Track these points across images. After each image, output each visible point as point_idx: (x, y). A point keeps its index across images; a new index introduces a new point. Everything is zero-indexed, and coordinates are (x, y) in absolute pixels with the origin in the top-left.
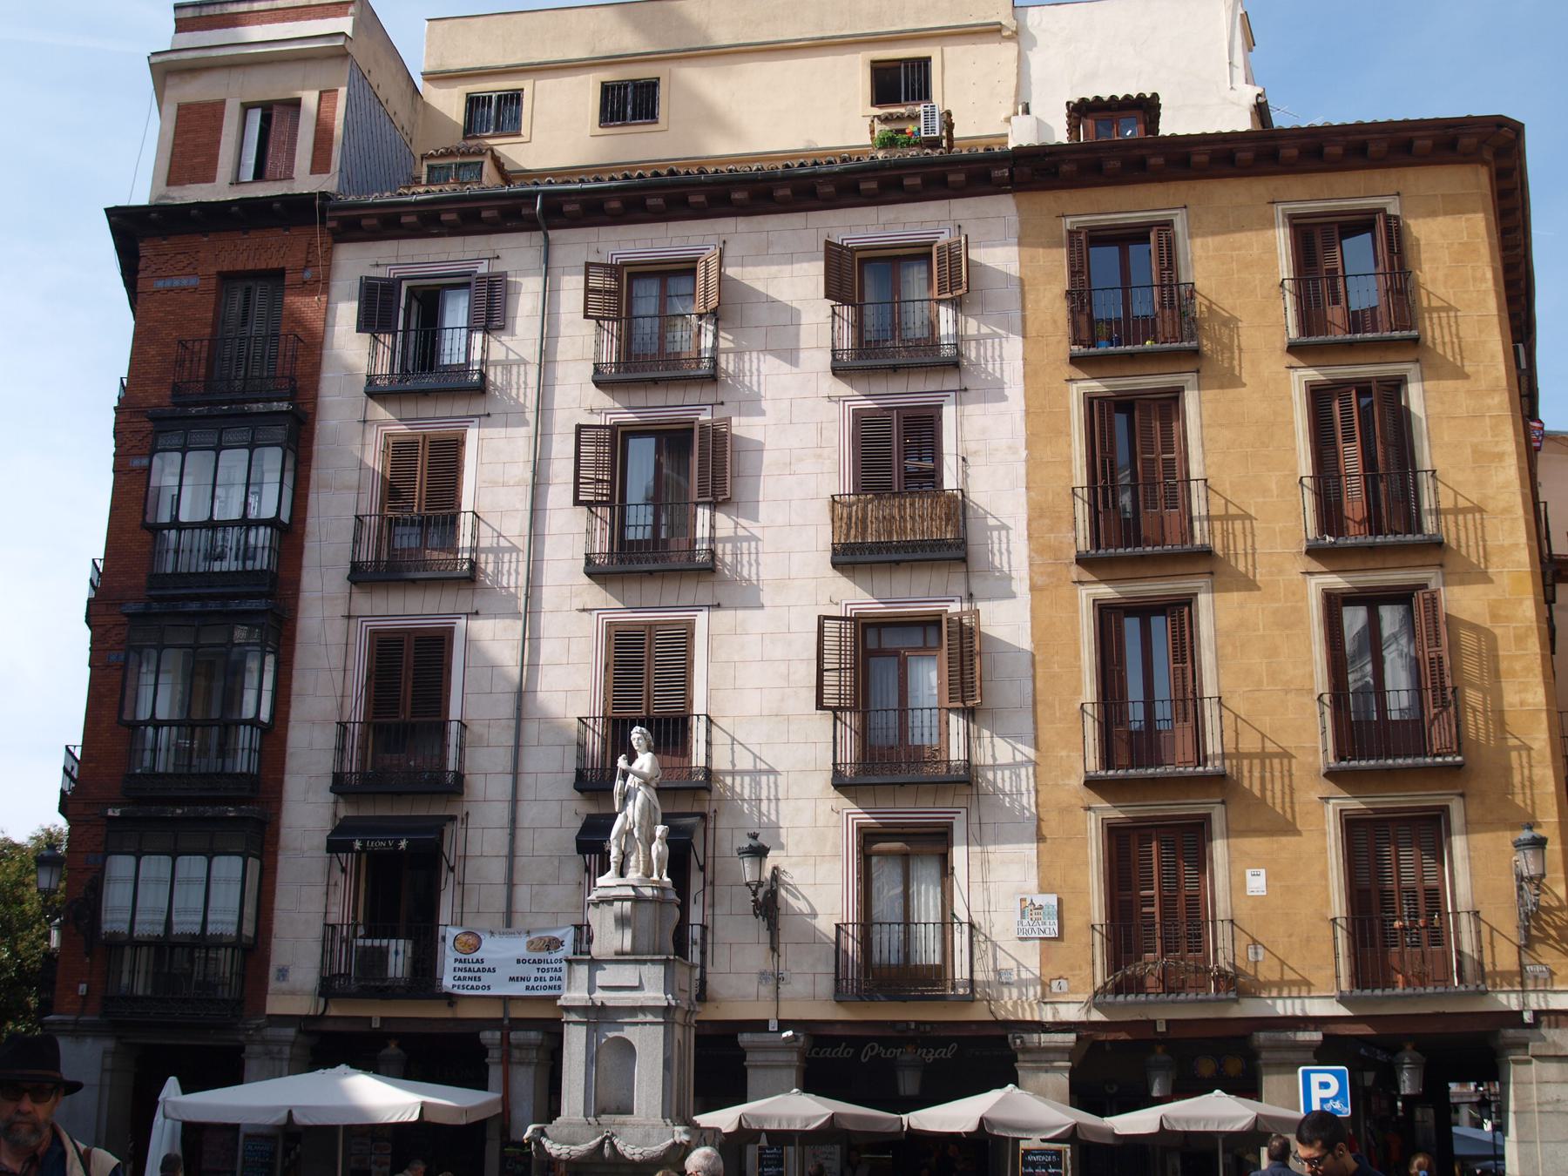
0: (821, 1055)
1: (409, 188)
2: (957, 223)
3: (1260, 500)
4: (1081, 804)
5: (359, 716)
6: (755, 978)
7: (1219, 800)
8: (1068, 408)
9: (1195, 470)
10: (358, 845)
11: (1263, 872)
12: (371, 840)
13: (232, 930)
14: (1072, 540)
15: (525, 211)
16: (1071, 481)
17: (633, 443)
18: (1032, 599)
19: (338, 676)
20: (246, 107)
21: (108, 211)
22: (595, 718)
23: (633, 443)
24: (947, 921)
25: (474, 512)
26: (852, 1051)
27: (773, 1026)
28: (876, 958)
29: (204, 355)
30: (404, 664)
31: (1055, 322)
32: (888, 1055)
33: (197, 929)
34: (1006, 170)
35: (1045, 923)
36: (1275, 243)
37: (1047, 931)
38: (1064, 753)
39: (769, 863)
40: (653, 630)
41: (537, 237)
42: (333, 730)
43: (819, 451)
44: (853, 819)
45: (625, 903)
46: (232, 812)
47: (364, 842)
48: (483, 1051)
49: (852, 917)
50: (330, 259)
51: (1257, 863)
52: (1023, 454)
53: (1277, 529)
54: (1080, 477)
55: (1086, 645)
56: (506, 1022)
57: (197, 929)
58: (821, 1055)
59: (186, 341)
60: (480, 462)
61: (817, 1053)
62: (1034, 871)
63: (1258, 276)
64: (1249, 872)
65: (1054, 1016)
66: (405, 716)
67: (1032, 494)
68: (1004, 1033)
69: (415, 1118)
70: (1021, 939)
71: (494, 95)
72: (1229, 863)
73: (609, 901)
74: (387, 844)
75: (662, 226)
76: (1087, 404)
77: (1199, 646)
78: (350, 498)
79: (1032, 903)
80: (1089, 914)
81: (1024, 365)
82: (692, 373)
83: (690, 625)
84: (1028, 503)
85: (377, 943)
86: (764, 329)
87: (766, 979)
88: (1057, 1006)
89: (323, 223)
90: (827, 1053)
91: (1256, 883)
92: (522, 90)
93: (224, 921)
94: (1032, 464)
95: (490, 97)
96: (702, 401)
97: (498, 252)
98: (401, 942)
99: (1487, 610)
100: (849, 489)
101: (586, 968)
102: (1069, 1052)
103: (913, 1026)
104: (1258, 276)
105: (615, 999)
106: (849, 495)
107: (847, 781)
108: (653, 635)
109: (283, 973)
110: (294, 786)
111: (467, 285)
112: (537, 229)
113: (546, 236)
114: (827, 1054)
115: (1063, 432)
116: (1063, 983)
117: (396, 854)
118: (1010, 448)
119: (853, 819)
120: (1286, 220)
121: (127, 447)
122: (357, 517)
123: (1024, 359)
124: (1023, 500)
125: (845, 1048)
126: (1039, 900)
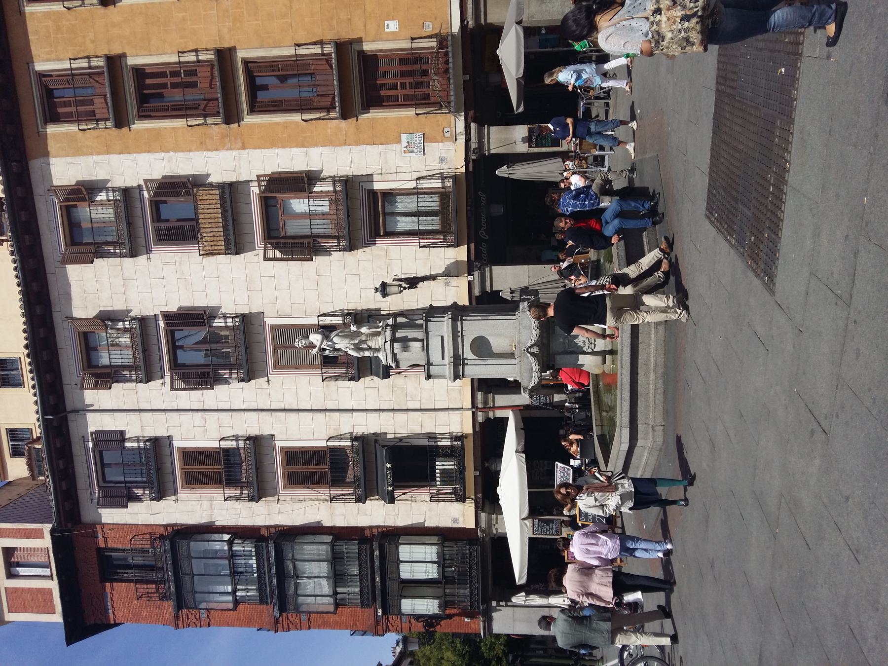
0: (486, 258)
1: (47, 487)
2: (46, 191)
3: (189, 23)
5: (327, 491)
7: (350, 46)
8: (145, 129)
9: (174, 59)
10: (390, 488)
11: (386, 22)
12: (388, 482)
13: (435, 549)
14: (217, 126)
15: (55, 424)
16: (184, 127)
17: (180, 361)
18: (250, 148)
19: (308, 503)
20: (10, 575)
21: (68, 645)
22: (322, 373)
23: (180, 361)
24: (416, 192)
25: (219, 441)
26: (483, 244)
28: (438, 227)
29: (145, 586)
30: (300, 471)
31: (98, 137)
32: (485, 226)
33: (435, 566)
34: (13, 164)
36: (44, 12)
37: (420, 139)
38: (329, 131)
39: (390, 282)
40: (277, 346)
41: (71, 417)
42: (334, 504)
43: (177, 264)
44: (368, 241)
45: (395, 346)
46: (377, 553)
47: (388, 485)
48: (488, 420)
49: (415, 240)
50: (91, 524)
51: (382, 27)
52: (172, 153)
53: (205, 13)
54: (181, 123)
55: (272, 119)
56: (474, 410)
57: (435, 566)
58: (486, 258)
59: (137, 596)
60: (194, 439)
61: (485, 260)
62: (389, 146)
63: (64, 22)
64: (387, 30)
65: (462, 135)
66: (326, 468)
67: (193, 149)
68: (471, 161)
69: (524, 455)
70: (424, 154)
71: (11, 443)
72: (382, 41)
73: (394, 356)
74: (389, 473)
75: (60, 351)
76: (141, 119)
77: (269, 57)
78: (216, 504)
79: (406, 147)
80: (411, 117)
81: (123, 154)
82: (139, 331)
83: (273, 327)
84: (198, 151)
85: (438, 475)
86: (113, 295)
87: (448, 283)
88: (457, 133)
89: (70, 531)
90: (484, 256)
91: (392, 26)
92: (6, 429)
93: (429, 552)
94: (177, 149)
95: (12, 445)
96: (155, 325)
97: (80, 438)
98: (437, 463)
100: (196, 247)
101: (431, 367)
102: (481, 125)
103: (469, 208)
104: (64, 22)
105: (449, 350)
106: (199, 247)
107: (348, 244)
108: (280, 346)
109: (455, 520)
110: (363, 520)
111: (101, 453)
112: (66, 416)
113: (70, 412)
114: (485, 255)
115: (158, 132)
116: (445, 130)
117: (393, 469)
118: (169, 161)
119: (368, 241)
120: (30, 5)
121: (197, 622)
122: (225, 500)
123: (120, 153)
124: (196, 153)
125: (482, 246)
126: (404, 144)
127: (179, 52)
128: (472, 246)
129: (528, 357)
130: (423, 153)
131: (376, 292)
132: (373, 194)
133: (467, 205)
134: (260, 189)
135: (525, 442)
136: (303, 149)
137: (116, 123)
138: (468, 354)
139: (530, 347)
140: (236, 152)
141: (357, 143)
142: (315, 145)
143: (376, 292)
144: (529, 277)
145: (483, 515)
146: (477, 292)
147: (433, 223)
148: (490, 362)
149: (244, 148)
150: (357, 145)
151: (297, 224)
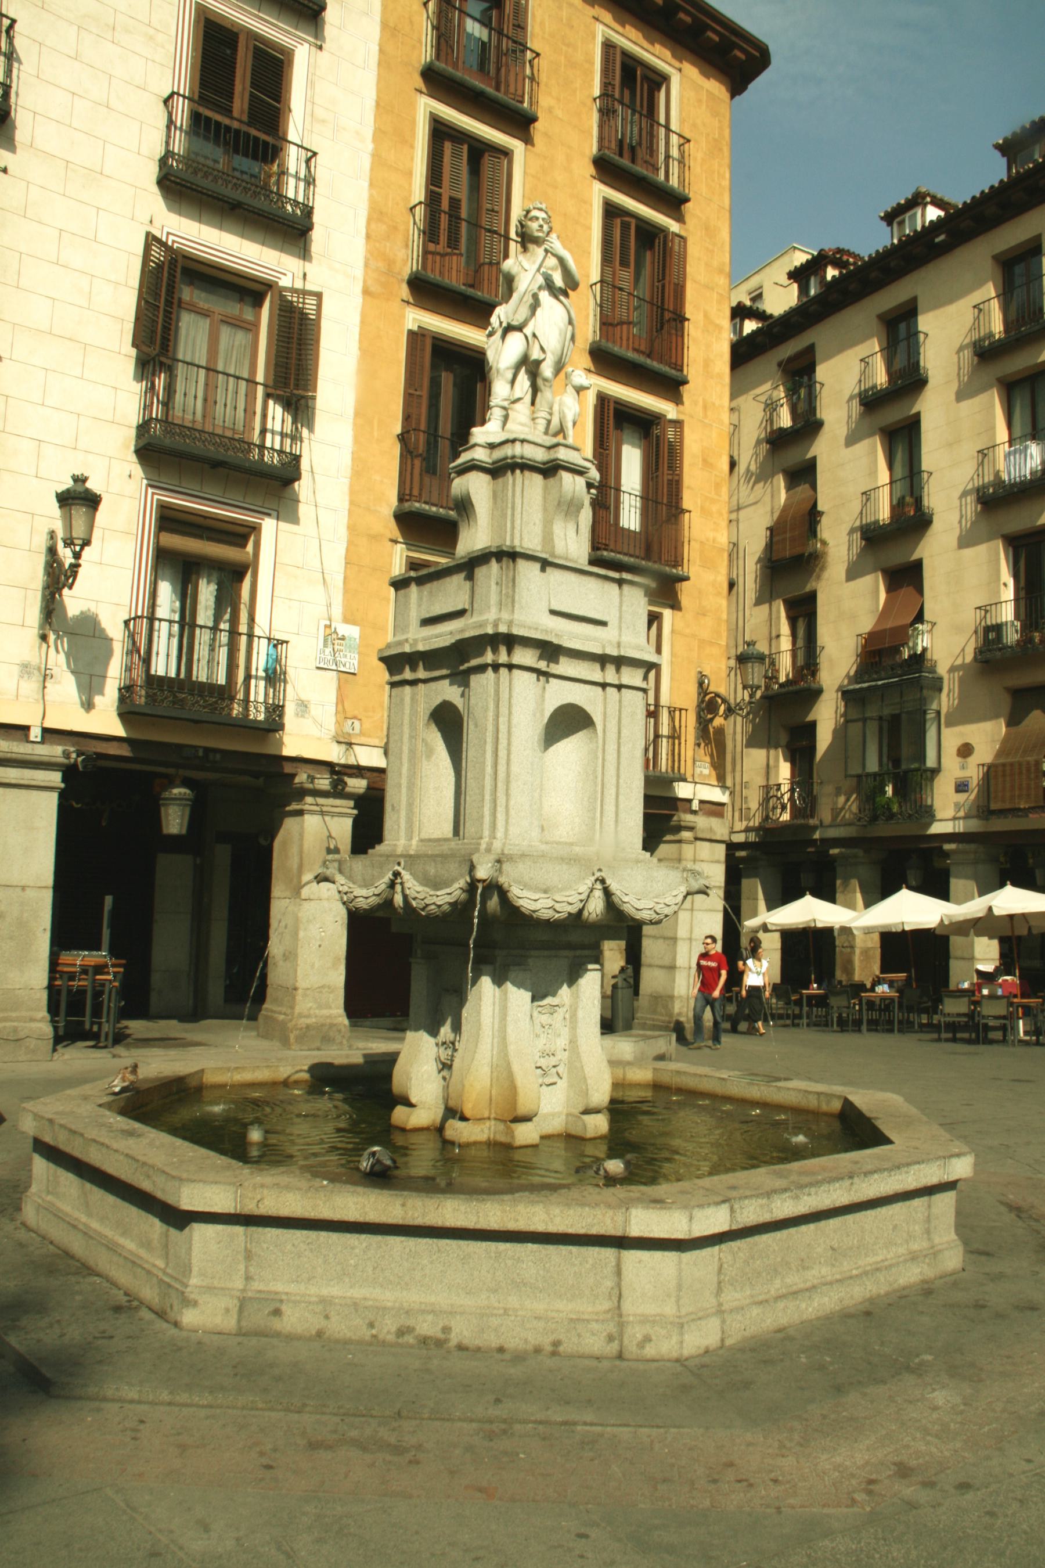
4: (390, 536)
6: (16, 670)
27: (35, 734)
35: (346, 656)
37: (347, 665)
38: (377, 477)
52: (370, 146)
70: (318, 668)
87: (29, 673)
99: (9, 987)
103: (201, 753)
115: (407, 142)
116: (357, 724)
126: (344, 629)
128: (125, 751)
130: (322, 665)
133: (207, 750)
134: (286, 289)
135: (440, 730)
136: (351, 412)
138: (559, 694)
140: (359, 272)
141: (352, 528)
142: (356, 440)
144: (23, 888)
147: (164, 665)
149: (366, 292)
150: (348, 527)
151: (198, 343)
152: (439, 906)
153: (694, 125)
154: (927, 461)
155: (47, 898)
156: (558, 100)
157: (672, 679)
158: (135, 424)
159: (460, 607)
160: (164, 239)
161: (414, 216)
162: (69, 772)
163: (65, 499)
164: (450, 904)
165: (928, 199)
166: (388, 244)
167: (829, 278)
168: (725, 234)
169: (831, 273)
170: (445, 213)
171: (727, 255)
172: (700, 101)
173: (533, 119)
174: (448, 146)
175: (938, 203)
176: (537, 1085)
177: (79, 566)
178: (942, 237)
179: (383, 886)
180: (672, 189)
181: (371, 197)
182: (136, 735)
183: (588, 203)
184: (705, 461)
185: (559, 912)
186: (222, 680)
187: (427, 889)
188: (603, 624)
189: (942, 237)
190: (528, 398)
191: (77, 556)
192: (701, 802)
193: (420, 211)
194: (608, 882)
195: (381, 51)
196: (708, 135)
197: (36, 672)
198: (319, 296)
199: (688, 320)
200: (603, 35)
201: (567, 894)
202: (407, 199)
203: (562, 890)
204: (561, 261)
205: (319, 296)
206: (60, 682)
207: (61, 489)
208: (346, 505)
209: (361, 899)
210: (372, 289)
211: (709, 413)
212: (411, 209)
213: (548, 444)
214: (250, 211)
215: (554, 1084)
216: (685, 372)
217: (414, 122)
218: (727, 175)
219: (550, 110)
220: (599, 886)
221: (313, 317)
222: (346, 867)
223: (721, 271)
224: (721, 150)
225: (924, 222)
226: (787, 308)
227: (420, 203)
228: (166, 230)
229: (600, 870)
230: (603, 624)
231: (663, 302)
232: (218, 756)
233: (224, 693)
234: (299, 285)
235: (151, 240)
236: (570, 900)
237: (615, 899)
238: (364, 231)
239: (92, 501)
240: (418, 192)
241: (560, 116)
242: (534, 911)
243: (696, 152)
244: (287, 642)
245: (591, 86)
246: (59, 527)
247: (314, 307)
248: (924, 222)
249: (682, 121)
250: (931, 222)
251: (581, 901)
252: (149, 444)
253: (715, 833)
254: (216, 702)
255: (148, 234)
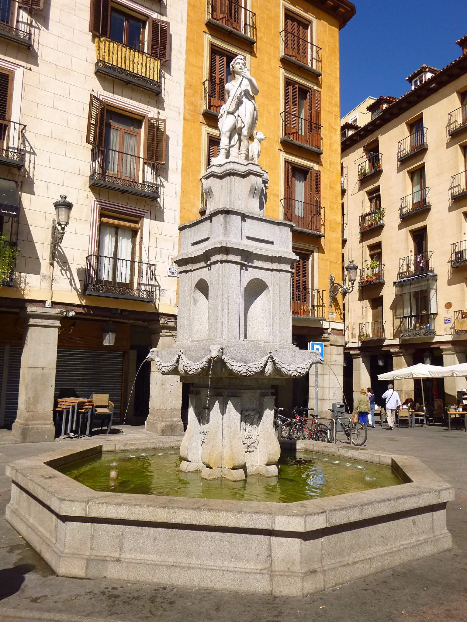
27: (48, 304)
38: (192, 197)
49: (94, 251)
52: (185, 56)
70: (169, 276)
87: (45, 279)
103: (119, 312)
127: (25, 126)
129: (262, 356)
130: (170, 275)
131: (61, 197)
132: (138, 219)
133: (122, 310)
134: (151, 118)
137: (211, 23)
138: (252, 274)
139: (274, 362)
142: (183, 182)
143: (61, 197)
145: (109, 241)
146: (32, 309)
148: (243, 302)
149: (185, 119)
150: (180, 217)
152: (196, 370)
153: (323, 42)
154: (428, 184)
155: (54, 372)
156: (264, 34)
157: (319, 278)
158: (89, 175)
159: (207, 237)
160: (98, 97)
161: (204, 85)
162: (64, 319)
163: (57, 205)
164: (201, 368)
165: (427, 70)
166: (194, 99)
167: (384, 108)
168: (338, 90)
169: (385, 106)
170: (217, 84)
171: (339, 98)
172: (325, 31)
173: (253, 43)
174: (218, 57)
175: (431, 71)
176: (243, 452)
177: (64, 233)
178: (434, 85)
179: (174, 362)
180: (314, 70)
181: (186, 78)
182: (89, 304)
183: (278, 78)
184: (330, 187)
185: (251, 372)
186: (128, 282)
187: (192, 362)
188: (272, 243)
189: (434, 85)
190: (238, 145)
191: (63, 229)
192: (333, 329)
193: (207, 84)
194: (275, 358)
195: (188, 15)
196: (329, 46)
197: (48, 278)
198: (165, 121)
199: (322, 127)
200: (283, 5)
201: (255, 363)
202: (201, 78)
203: (252, 362)
204: (250, 81)
205: (165, 121)
206: (58, 283)
207: (55, 201)
208: (179, 208)
209: (165, 367)
210: (187, 118)
211: (332, 166)
212: (203, 83)
213: (245, 164)
214: (134, 85)
215: (253, 451)
216: (321, 149)
217: (203, 46)
218: (338, 63)
219: (261, 39)
220: (270, 360)
221: (163, 130)
222: (160, 354)
223: (336, 105)
224: (335, 52)
225: (425, 79)
226: (367, 123)
227: (207, 80)
228: (99, 93)
229: (270, 353)
230: (272, 243)
231: (311, 120)
232: (127, 313)
233: (129, 286)
234: (156, 116)
235: (93, 97)
236: (256, 366)
237: (278, 366)
238: (183, 93)
239: (69, 206)
240: (206, 75)
241: (265, 41)
242: (239, 372)
243: (324, 54)
244: (155, 265)
245: (278, 28)
246: (55, 217)
247: (163, 126)
248: (425, 79)
249: (318, 40)
250: (429, 78)
251: (262, 367)
252: (94, 183)
253: (338, 342)
254: (125, 290)
255: (91, 95)
